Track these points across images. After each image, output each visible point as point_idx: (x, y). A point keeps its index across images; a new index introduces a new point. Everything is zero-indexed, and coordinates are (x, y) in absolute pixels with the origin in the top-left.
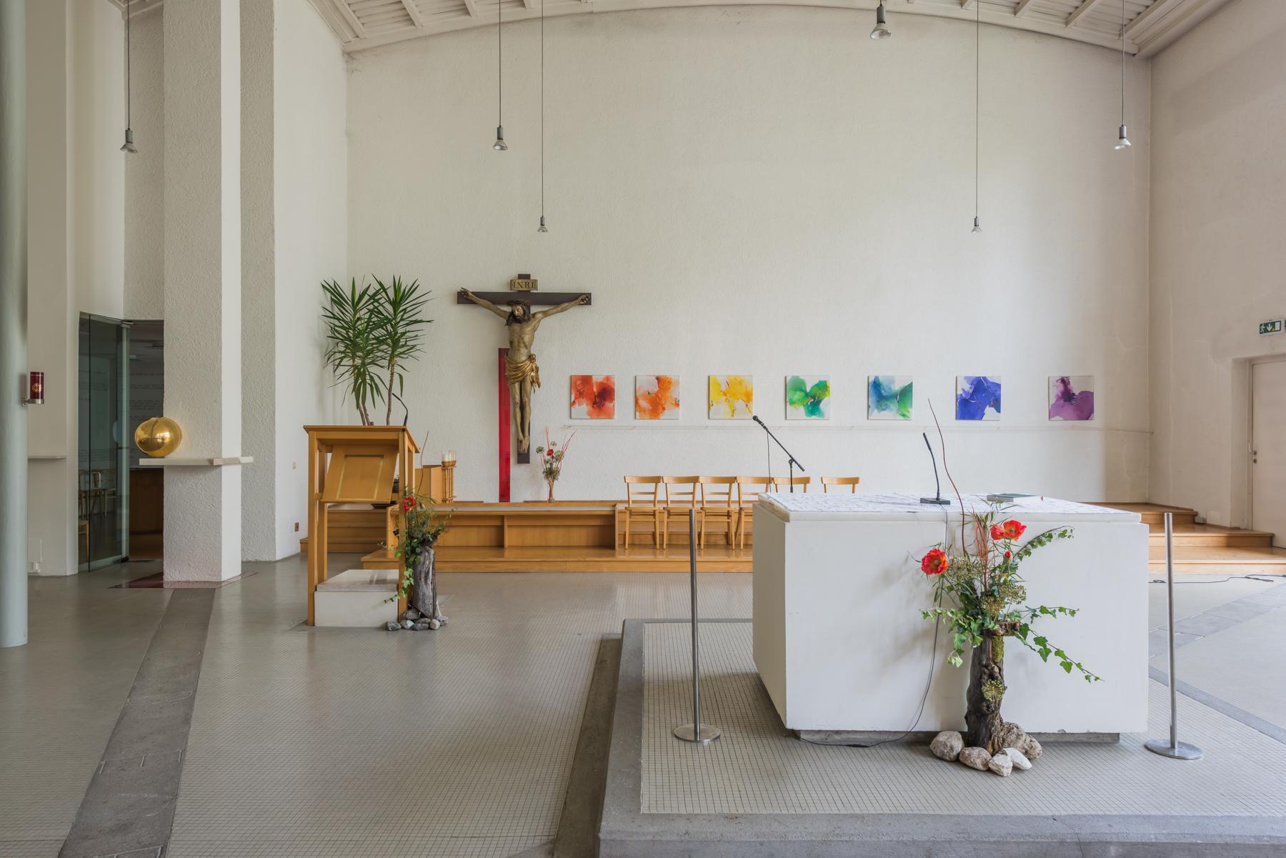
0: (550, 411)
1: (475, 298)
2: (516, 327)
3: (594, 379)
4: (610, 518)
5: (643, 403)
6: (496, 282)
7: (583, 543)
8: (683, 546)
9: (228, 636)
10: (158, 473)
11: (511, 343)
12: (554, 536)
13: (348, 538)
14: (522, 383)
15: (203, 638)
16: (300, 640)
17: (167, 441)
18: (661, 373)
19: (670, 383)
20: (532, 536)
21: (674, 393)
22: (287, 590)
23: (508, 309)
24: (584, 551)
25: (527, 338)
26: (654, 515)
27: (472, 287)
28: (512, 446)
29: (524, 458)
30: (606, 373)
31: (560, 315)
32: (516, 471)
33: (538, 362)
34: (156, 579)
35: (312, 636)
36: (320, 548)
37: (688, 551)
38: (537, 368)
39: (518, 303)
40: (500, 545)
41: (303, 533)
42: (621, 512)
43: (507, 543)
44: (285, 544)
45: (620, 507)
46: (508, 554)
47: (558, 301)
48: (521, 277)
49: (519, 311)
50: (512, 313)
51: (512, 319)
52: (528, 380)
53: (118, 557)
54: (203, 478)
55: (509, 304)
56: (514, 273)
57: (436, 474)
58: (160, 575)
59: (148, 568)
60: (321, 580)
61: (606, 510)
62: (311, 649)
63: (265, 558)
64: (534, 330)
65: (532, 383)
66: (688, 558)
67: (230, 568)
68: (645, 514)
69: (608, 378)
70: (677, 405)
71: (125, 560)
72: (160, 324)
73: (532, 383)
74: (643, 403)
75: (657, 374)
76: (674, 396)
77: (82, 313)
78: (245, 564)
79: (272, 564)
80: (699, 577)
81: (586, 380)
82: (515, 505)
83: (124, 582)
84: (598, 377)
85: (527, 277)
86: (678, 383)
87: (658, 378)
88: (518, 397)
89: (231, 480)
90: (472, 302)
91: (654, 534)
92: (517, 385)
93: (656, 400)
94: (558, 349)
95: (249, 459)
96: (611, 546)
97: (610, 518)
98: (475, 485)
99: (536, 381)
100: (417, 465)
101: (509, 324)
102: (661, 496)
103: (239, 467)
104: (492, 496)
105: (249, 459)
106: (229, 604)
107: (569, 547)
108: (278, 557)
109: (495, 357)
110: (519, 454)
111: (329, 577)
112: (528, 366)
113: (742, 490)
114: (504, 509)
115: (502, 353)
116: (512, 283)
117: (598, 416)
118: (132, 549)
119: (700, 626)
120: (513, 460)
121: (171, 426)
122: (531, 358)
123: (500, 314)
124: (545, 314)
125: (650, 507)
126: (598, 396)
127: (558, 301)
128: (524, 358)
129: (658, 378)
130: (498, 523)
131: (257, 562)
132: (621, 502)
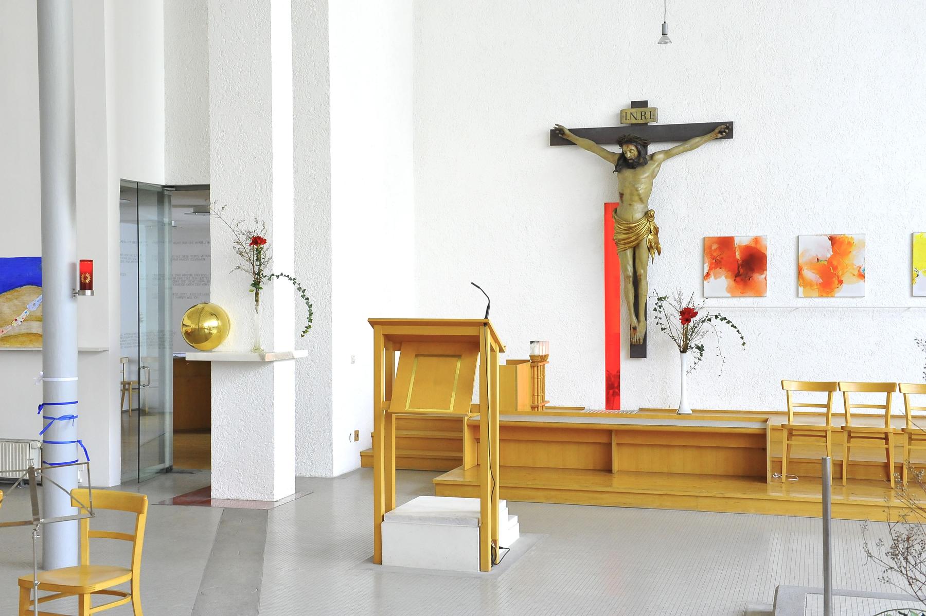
0: (675, 274)
1: (573, 138)
2: (628, 173)
3: (737, 241)
4: (761, 437)
5: (809, 274)
6: (602, 114)
7: (720, 471)
8: (94, 488)
9: (282, 570)
10: (205, 367)
11: (622, 195)
12: (681, 460)
13: (424, 452)
14: (635, 249)
15: (259, 572)
16: (362, 581)
17: (214, 332)
18: (836, 232)
19: (850, 244)
20: (649, 459)
21: (855, 259)
22: (349, 516)
23: (617, 149)
24: (724, 483)
25: (642, 188)
26: (886, 439)
27: (569, 123)
28: (626, 338)
29: (639, 350)
30: (753, 233)
31: (689, 155)
32: (628, 367)
33: (658, 221)
34: (203, 495)
35: (378, 578)
36: (387, 462)
37: (820, 488)
38: (657, 230)
39: (630, 141)
40: (607, 469)
41: (365, 442)
42: (775, 429)
43: (615, 467)
44: (344, 458)
45: (774, 422)
46: (618, 483)
47: (685, 135)
48: (635, 104)
49: (631, 152)
50: (622, 156)
51: (623, 163)
52: (644, 245)
53: (161, 466)
54: (252, 377)
55: (620, 143)
56: (625, 102)
57: (524, 371)
58: (208, 489)
59: (191, 481)
60: (389, 508)
61: (753, 426)
62: (378, 595)
63: (320, 472)
64: (653, 176)
65: (650, 249)
66: (819, 497)
67: (283, 488)
68: (870, 436)
69: (757, 240)
70: (862, 276)
71: (168, 470)
72: (207, 187)
73: (650, 249)
74: (809, 274)
75: (830, 233)
76: (858, 262)
77: (122, 180)
78: (299, 480)
79: (328, 481)
80: (833, 525)
81: (726, 243)
82: (629, 415)
83: (168, 497)
84: (742, 237)
85: (644, 104)
86: (863, 244)
87: (832, 239)
88: (630, 269)
89: (284, 376)
90: (569, 143)
91: (886, 466)
92: (629, 253)
93: (830, 270)
94: (687, 199)
95: (303, 354)
96: (761, 478)
97: (761, 437)
98: (574, 387)
99: (654, 247)
100: (502, 360)
101: (618, 169)
102: (897, 407)
103: (293, 362)
104: (596, 400)
105: (303, 354)
106: (282, 530)
107: (670, 474)
108: (337, 472)
109: (599, 214)
110: (632, 346)
111: (397, 506)
112: (644, 227)
113: (850, 402)
114: (612, 421)
115: (611, 211)
116: (623, 114)
117: (743, 294)
118: (176, 455)
119: (836, 601)
120: (624, 352)
121: (215, 314)
122: (648, 215)
123: (608, 156)
124: (668, 154)
125: (880, 425)
126: (742, 265)
127: (685, 135)
128: (638, 215)
129: (832, 239)
130: (603, 439)
131: (312, 478)
132: (777, 413)
